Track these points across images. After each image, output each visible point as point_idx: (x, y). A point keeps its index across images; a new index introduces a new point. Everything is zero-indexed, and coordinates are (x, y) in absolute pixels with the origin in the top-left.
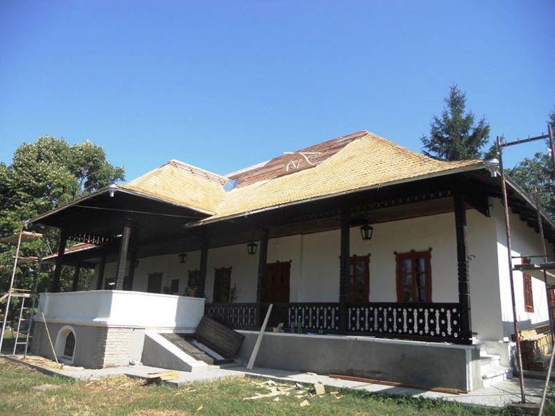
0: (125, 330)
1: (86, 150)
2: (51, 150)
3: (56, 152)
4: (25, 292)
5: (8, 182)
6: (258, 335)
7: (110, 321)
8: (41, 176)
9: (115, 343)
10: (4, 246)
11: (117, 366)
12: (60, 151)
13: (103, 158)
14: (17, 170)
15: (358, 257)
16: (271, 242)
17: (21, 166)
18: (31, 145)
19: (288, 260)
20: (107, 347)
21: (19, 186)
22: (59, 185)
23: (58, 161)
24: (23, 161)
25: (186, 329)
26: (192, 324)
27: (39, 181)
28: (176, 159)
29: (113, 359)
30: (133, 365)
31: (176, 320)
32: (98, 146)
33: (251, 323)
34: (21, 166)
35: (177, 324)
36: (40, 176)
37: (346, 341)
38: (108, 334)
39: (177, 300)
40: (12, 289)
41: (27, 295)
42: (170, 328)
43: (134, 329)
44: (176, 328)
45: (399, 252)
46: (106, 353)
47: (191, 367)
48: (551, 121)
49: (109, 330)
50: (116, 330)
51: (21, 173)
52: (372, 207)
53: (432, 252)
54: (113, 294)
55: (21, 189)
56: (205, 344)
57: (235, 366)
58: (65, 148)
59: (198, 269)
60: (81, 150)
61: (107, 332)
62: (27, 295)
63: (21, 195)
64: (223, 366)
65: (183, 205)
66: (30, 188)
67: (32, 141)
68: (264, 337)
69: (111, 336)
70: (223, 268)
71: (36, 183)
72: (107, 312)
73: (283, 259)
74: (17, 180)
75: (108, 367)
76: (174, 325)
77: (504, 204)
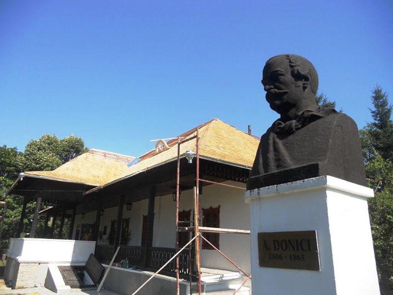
0: (33, 264)
1: (69, 141)
3: (49, 144)
5: (20, 165)
6: (108, 267)
9: (25, 273)
11: (25, 288)
12: (53, 143)
14: (25, 157)
15: (186, 212)
16: (157, 199)
18: (36, 141)
19: (189, 210)
20: (18, 275)
23: (50, 150)
24: (29, 151)
25: (80, 262)
26: (83, 260)
27: (37, 164)
28: (94, 148)
29: (23, 283)
30: (36, 287)
33: (169, 254)
35: (72, 260)
37: (140, 274)
38: (20, 267)
43: (39, 264)
44: (72, 262)
45: (205, 208)
46: (18, 279)
47: (57, 290)
48: (374, 95)
49: (21, 264)
50: (26, 264)
53: (221, 209)
54: (25, 241)
55: (28, 169)
56: (88, 274)
57: (87, 290)
58: (56, 141)
59: (116, 219)
60: (66, 141)
61: (19, 266)
64: (84, 289)
65: (79, 181)
68: (111, 269)
70: (211, 207)
71: (35, 165)
74: (25, 164)
75: (19, 288)
76: (70, 260)
77: (213, 184)
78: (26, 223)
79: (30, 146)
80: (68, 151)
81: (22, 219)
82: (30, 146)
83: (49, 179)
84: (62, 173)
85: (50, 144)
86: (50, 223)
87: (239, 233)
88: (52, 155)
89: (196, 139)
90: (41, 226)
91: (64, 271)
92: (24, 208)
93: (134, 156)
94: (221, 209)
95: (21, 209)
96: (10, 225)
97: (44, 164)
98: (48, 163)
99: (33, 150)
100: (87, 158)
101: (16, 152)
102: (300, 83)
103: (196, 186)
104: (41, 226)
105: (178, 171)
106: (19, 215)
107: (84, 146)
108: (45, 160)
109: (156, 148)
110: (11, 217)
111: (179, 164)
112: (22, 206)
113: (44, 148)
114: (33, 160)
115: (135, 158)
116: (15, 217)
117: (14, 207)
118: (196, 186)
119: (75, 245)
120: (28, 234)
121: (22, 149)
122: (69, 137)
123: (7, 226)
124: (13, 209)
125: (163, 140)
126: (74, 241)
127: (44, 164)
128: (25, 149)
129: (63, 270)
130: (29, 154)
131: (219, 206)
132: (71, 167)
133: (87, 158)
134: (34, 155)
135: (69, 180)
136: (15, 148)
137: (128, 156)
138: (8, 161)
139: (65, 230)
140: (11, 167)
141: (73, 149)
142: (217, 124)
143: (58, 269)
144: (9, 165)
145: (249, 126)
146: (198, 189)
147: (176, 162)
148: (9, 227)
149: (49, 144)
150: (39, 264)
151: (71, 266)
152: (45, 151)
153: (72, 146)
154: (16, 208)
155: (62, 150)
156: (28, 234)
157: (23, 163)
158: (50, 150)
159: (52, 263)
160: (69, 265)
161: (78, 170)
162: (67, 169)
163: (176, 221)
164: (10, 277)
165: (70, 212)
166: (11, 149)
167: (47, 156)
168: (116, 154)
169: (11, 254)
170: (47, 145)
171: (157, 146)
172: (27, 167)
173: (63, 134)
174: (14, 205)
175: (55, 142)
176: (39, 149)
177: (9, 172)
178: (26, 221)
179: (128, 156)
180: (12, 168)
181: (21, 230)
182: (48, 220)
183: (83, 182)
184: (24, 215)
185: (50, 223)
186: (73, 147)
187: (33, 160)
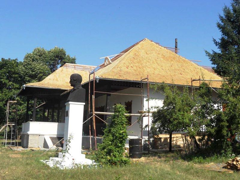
2: (38, 55)
3: (40, 56)
4: (13, 123)
7: (29, 133)
8: (34, 69)
10: (22, 103)
12: (42, 55)
13: (65, 54)
14: (24, 67)
17: (26, 65)
18: (30, 54)
20: (29, 141)
21: (26, 74)
22: (41, 73)
23: (41, 60)
25: (54, 135)
27: (33, 71)
31: (58, 132)
32: (61, 48)
34: (26, 65)
36: (33, 69)
37: (87, 137)
39: (57, 124)
40: (8, 123)
41: (14, 124)
42: (55, 135)
43: (39, 135)
44: (57, 135)
49: (30, 136)
51: (26, 69)
52: (114, 84)
54: (30, 123)
55: (27, 76)
60: (52, 52)
62: (14, 124)
63: (27, 79)
65: (57, 88)
66: (30, 75)
67: (31, 51)
69: (30, 138)
71: (32, 73)
72: (28, 130)
73: (130, 101)
74: (25, 72)
76: (56, 134)
78: (31, 114)
79: (27, 58)
80: (54, 60)
81: (27, 112)
82: (26, 58)
83: (39, 87)
84: (47, 83)
85: (40, 55)
86: (46, 114)
87: (136, 116)
88: (43, 64)
89: (93, 74)
90: (41, 116)
91: (53, 139)
92: (28, 104)
93: (96, 66)
94: (132, 102)
95: (26, 105)
96: (20, 115)
97: (37, 72)
98: (40, 70)
99: (29, 61)
100: (62, 70)
101: (18, 63)
102: (75, 81)
103: (93, 95)
104: (41, 116)
105: (90, 87)
106: (25, 109)
107: (65, 54)
108: (38, 68)
109: (105, 62)
110: (20, 111)
111: (90, 84)
112: (26, 102)
113: (37, 59)
114: (30, 68)
115: (96, 67)
116: (23, 110)
117: (21, 103)
118: (93, 95)
119: (58, 126)
120: (31, 119)
121: (21, 59)
122: (54, 49)
123: (18, 117)
124: (21, 104)
125: (108, 57)
126: (57, 123)
127: (37, 72)
128: (23, 60)
129: (52, 139)
130: (26, 64)
131: (132, 101)
132: (52, 78)
133: (62, 70)
134: (30, 64)
135: (51, 87)
136: (16, 59)
137: (91, 66)
138: (13, 70)
139: (56, 117)
140: (16, 74)
141: (59, 59)
142: (146, 44)
143: (50, 139)
144: (15, 73)
145: (176, 39)
146: (94, 96)
147: (93, 81)
148: (20, 117)
149: (40, 56)
150: (39, 135)
151: (57, 137)
152: (38, 61)
153: (57, 55)
154: (23, 104)
155: (50, 60)
156: (31, 119)
157: (23, 71)
158: (41, 60)
159: (46, 135)
160: (56, 136)
161: (57, 80)
162: (50, 80)
163: (88, 110)
164: (25, 145)
165: (56, 106)
166: (14, 60)
167: (39, 66)
168: (82, 65)
169: (24, 132)
170: (38, 57)
171: (105, 61)
172: (26, 74)
173: (49, 46)
174: (21, 102)
175: (44, 54)
176: (33, 60)
177: (15, 78)
178: (30, 113)
179: (91, 66)
180: (16, 75)
181: (27, 118)
182: (45, 112)
183: (59, 88)
184: (28, 109)
185: (46, 114)
186: (57, 57)
187: (30, 68)
